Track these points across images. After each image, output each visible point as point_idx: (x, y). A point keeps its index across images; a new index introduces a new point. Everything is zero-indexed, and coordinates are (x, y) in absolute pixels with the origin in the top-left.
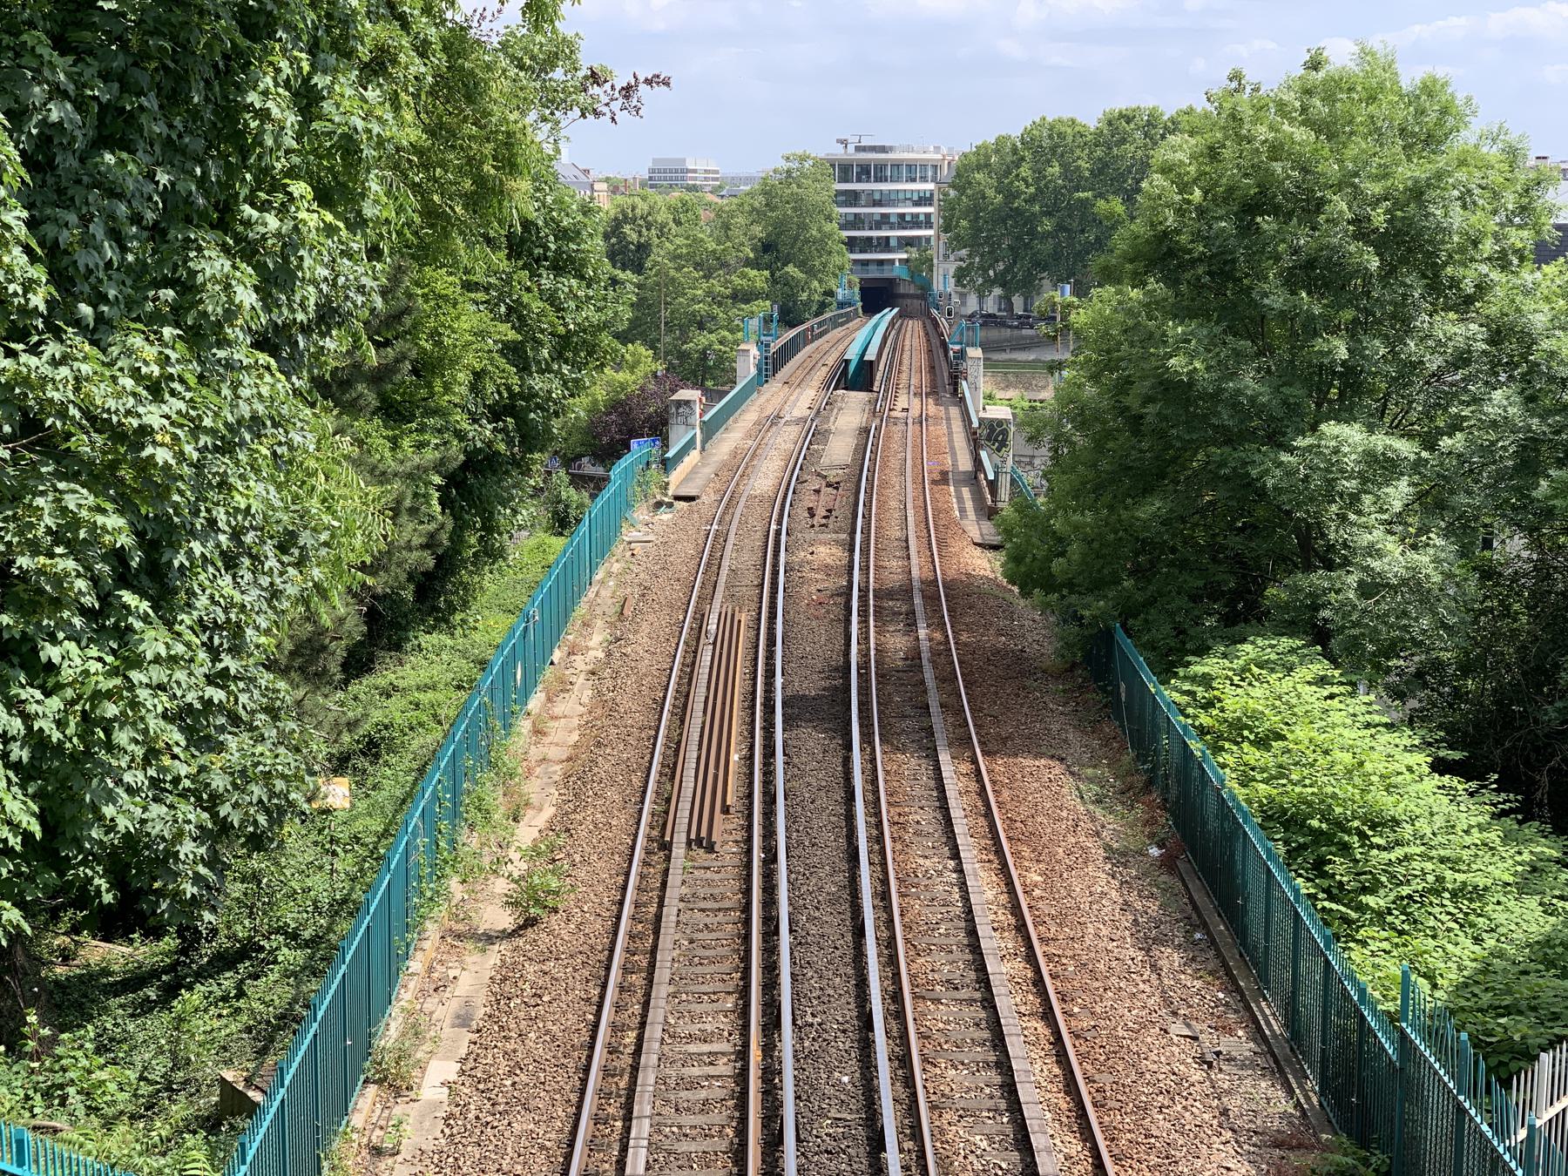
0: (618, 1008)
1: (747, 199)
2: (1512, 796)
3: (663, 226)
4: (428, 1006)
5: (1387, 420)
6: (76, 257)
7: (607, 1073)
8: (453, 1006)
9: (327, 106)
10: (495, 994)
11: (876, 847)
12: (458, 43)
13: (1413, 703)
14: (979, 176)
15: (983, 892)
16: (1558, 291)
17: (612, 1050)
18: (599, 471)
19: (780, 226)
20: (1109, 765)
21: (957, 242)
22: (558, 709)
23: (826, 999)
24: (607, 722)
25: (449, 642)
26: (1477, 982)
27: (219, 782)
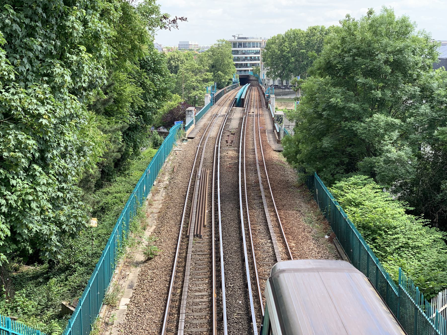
0: (175, 283)
1: (207, 53)
2: (428, 220)
3: (183, 60)
4: (121, 283)
5: (392, 114)
6: (19, 67)
7: (172, 301)
8: (128, 283)
9: (90, 24)
10: (139, 279)
11: (248, 236)
12: (125, 8)
13: (399, 194)
14: (273, 46)
15: (278, 249)
16: (440, 77)
17: (173, 294)
18: (165, 130)
19: (217, 61)
20: (313, 213)
21: (267, 65)
22: (156, 198)
23: (234, 280)
24: (170, 202)
25: (124, 179)
26: (419, 273)
27: (63, 219)
